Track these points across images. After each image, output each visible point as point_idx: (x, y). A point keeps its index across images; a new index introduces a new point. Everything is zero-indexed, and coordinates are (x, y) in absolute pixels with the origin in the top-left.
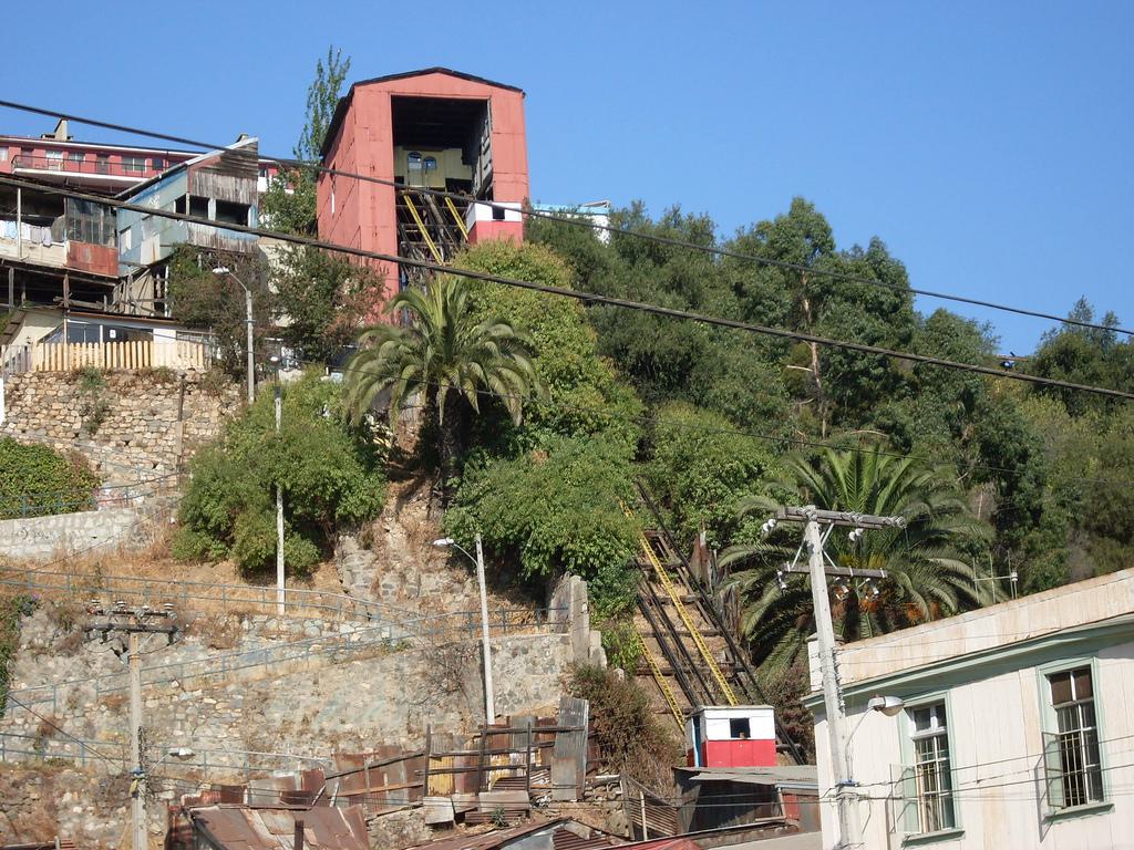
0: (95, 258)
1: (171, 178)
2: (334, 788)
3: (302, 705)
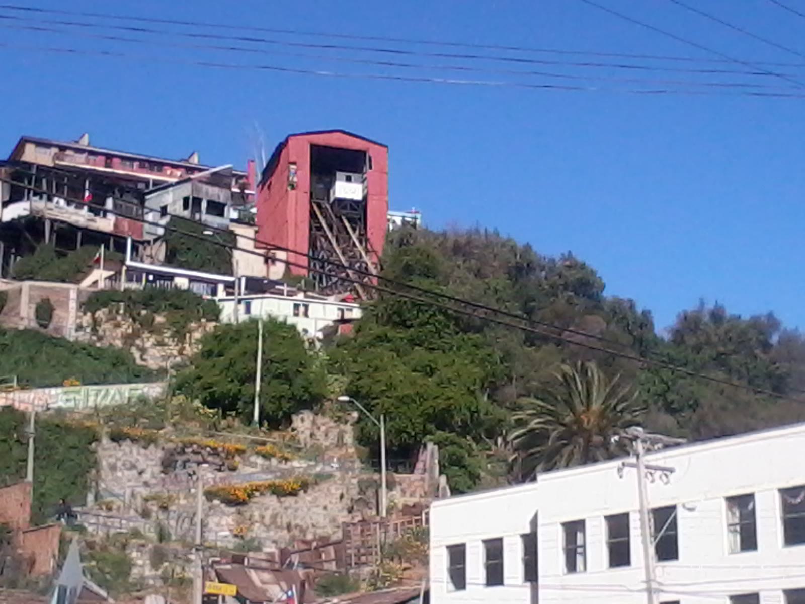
2: (295, 558)
3: (271, 508)
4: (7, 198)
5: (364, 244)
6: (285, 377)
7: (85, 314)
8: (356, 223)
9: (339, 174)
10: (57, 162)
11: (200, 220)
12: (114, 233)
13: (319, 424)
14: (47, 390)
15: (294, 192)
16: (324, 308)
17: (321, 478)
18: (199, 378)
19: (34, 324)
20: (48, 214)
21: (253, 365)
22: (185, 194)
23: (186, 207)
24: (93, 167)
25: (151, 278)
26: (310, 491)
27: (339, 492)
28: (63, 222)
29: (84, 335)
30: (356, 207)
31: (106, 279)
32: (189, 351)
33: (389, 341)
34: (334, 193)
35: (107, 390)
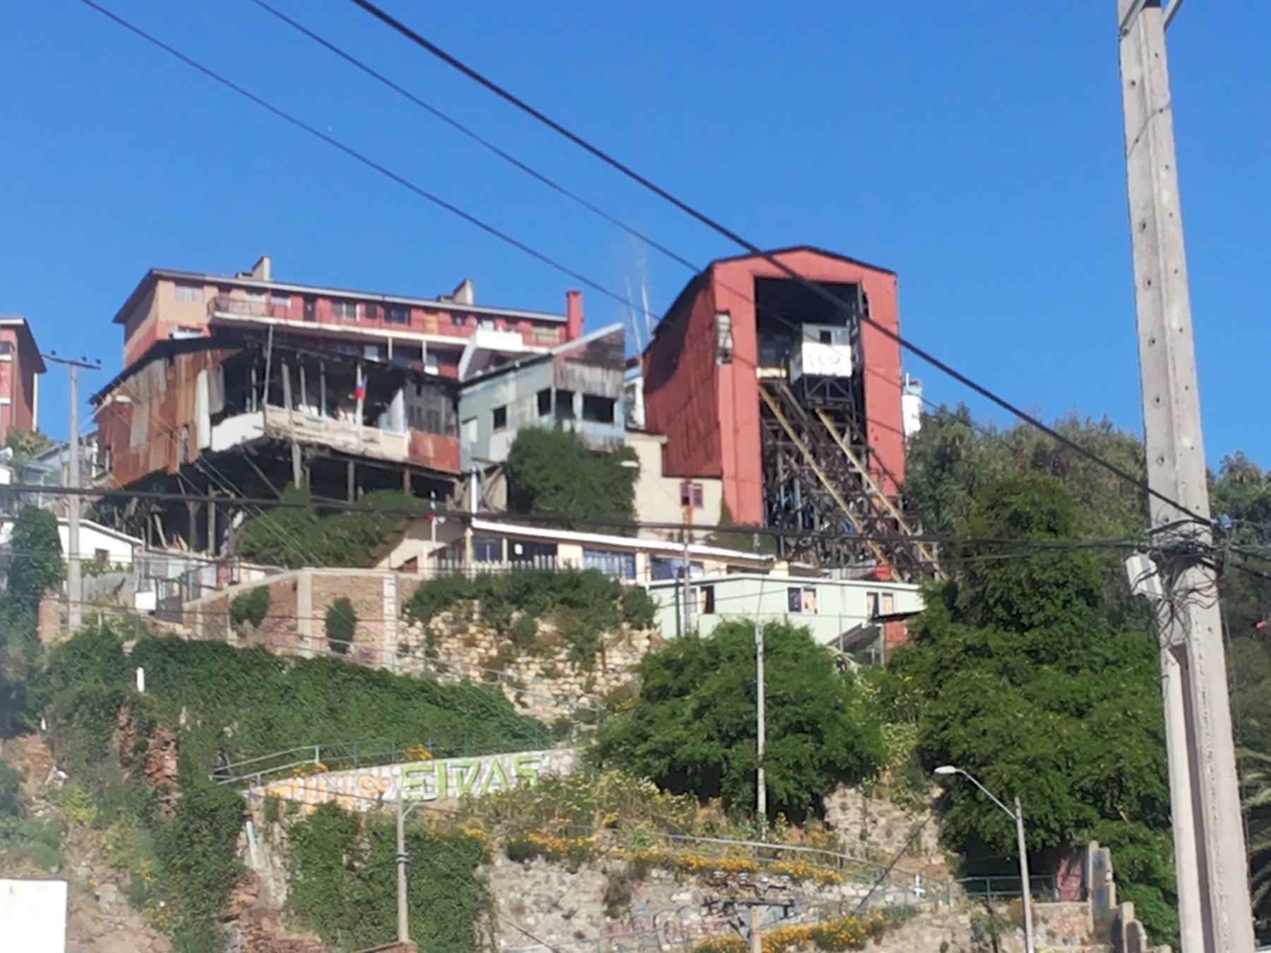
0: (436, 451)
1: (497, 380)
4: (219, 408)
5: (864, 459)
6: (805, 727)
7: (411, 624)
8: (843, 420)
9: (811, 330)
10: (218, 314)
11: (572, 430)
12: (410, 462)
13: (876, 816)
14: (375, 770)
15: (728, 367)
16: (843, 594)
17: (901, 916)
18: (645, 738)
19: (325, 649)
20: (297, 435)
21: (751, 707)
22: (542, 386)
23: (543, 407)
24: (283, 321)
25: (519, 549)
26: (885, 941)
27: (939, 940)
28: (322, 447)
29: (413, 663)
30: (843, 391)
31: (431, 555)
32: (603, 684)
33: (990, 656)
34: (800, 364)
35: (480, 765)
